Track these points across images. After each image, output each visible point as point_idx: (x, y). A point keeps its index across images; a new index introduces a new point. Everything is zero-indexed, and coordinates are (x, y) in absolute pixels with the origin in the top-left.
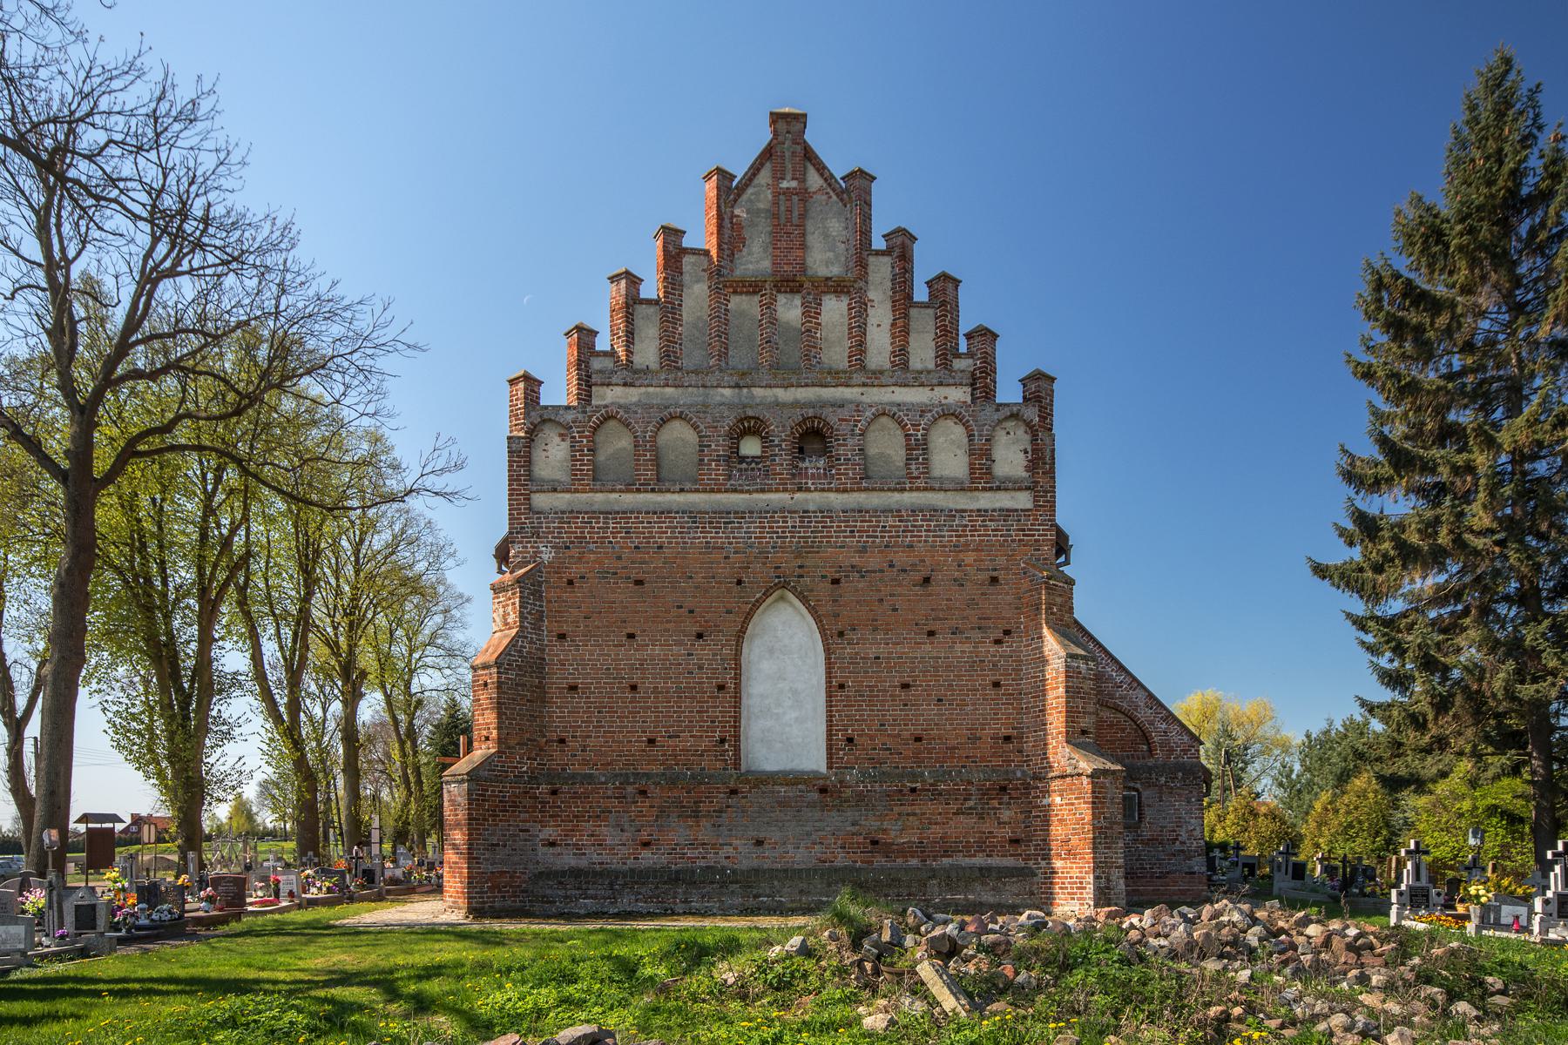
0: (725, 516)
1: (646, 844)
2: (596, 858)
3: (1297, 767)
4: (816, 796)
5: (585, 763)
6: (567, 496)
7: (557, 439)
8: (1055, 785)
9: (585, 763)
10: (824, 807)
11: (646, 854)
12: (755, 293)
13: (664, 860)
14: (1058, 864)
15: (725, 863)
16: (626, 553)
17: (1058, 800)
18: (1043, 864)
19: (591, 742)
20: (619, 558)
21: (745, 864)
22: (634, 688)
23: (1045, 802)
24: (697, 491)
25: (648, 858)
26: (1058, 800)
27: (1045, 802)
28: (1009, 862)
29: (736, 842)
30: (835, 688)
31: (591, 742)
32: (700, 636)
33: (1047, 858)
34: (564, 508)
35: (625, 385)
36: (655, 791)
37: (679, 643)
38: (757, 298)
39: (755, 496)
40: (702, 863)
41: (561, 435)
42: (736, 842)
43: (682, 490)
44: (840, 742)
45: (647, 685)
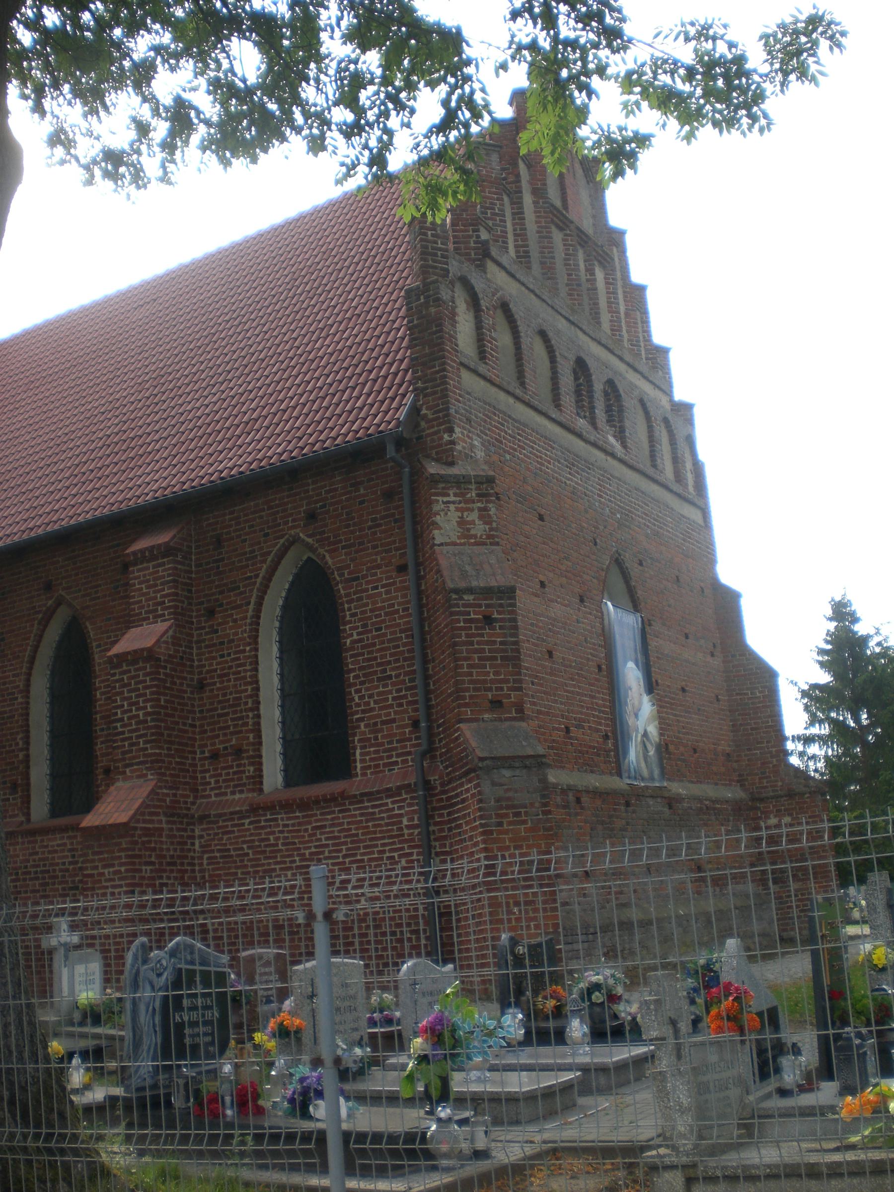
22: (550, 654)
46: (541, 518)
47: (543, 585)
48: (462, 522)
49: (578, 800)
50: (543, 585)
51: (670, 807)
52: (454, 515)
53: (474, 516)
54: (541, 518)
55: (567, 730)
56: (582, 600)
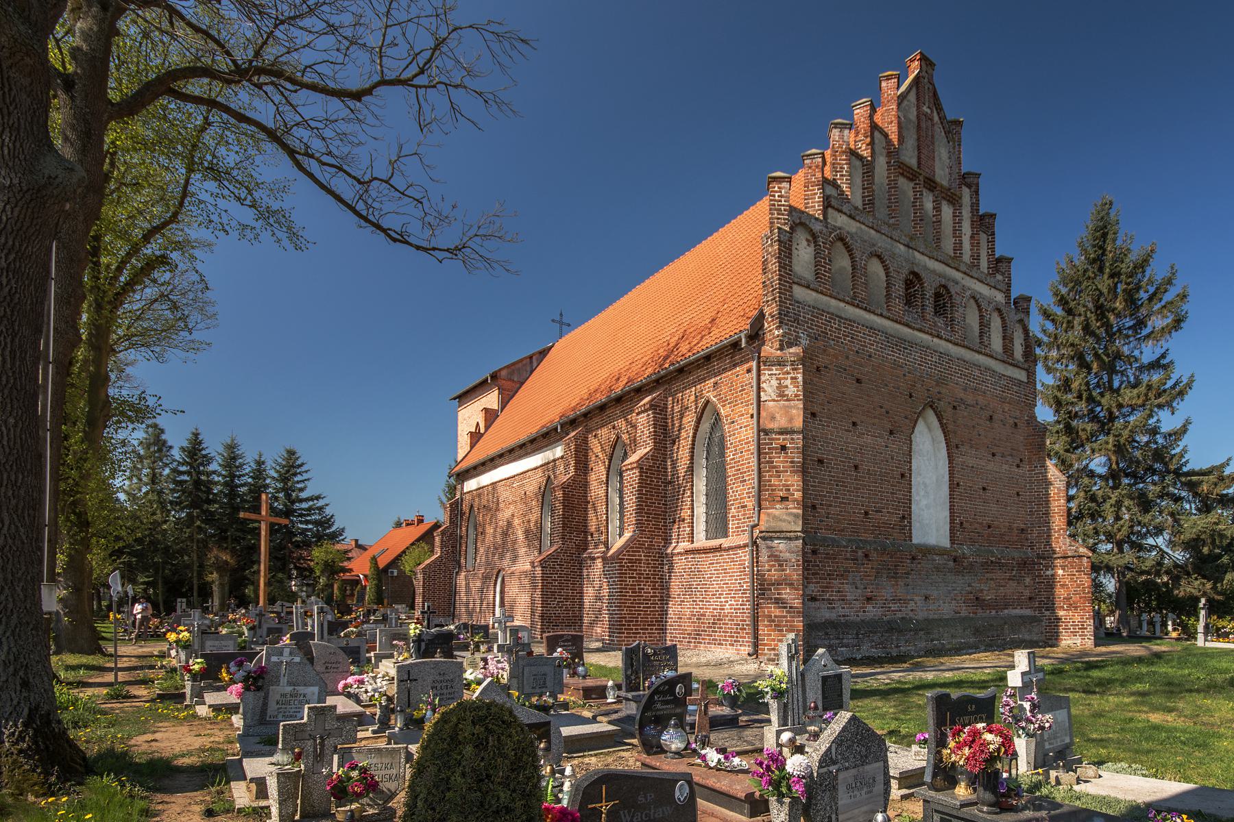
0: (902, 344)
1: (869, 599)
2: (841, 612)
3: (225, 557)
4: (951, 563)
5: (828, 528)
6: (814, 294)
7: (805, 243)
8: (1058, 562)
9: (828, 528)
10: (958, 573)
11: (869, 607)
12: (911, 180)
13: (879, 612)
14: (1061, 613)
15: (911, 614)
16: (852, 355)
17: (1060, 572)
18: (1047, 613)
19: (832, 510)
20: (847, 358)
21: (921, 615)
22: (856, 467)
23: (1049, 573)
24: (888, 318)
25: (872, 611)
26: (1060, 572)
27: (1049, 573)
28: (1028, 612)
29: (916, 598)
30: (954, 486)
31: (832, 510)
32: (891, 433)
33: (1052, 608)
34: (811, 303)
35: (850, 216)
36: (874, 555)
37: (881, 436)
38: (912, 185)
39: (916, 333)
40: (899, 615)
41: (807, 240)
42: (916, 598)
43: (881, 315)
44: (956, 526)
45: (864, 467)
46: (858, 381)
47: (854, 424)
48: (780, 387)
49: (866, 556)
50: (854, 424)
51: (955, 561)
52: (774, 383)
53: (788, 382)
54: (858, 381)
55: (866, 513)
56: (891, 433)
